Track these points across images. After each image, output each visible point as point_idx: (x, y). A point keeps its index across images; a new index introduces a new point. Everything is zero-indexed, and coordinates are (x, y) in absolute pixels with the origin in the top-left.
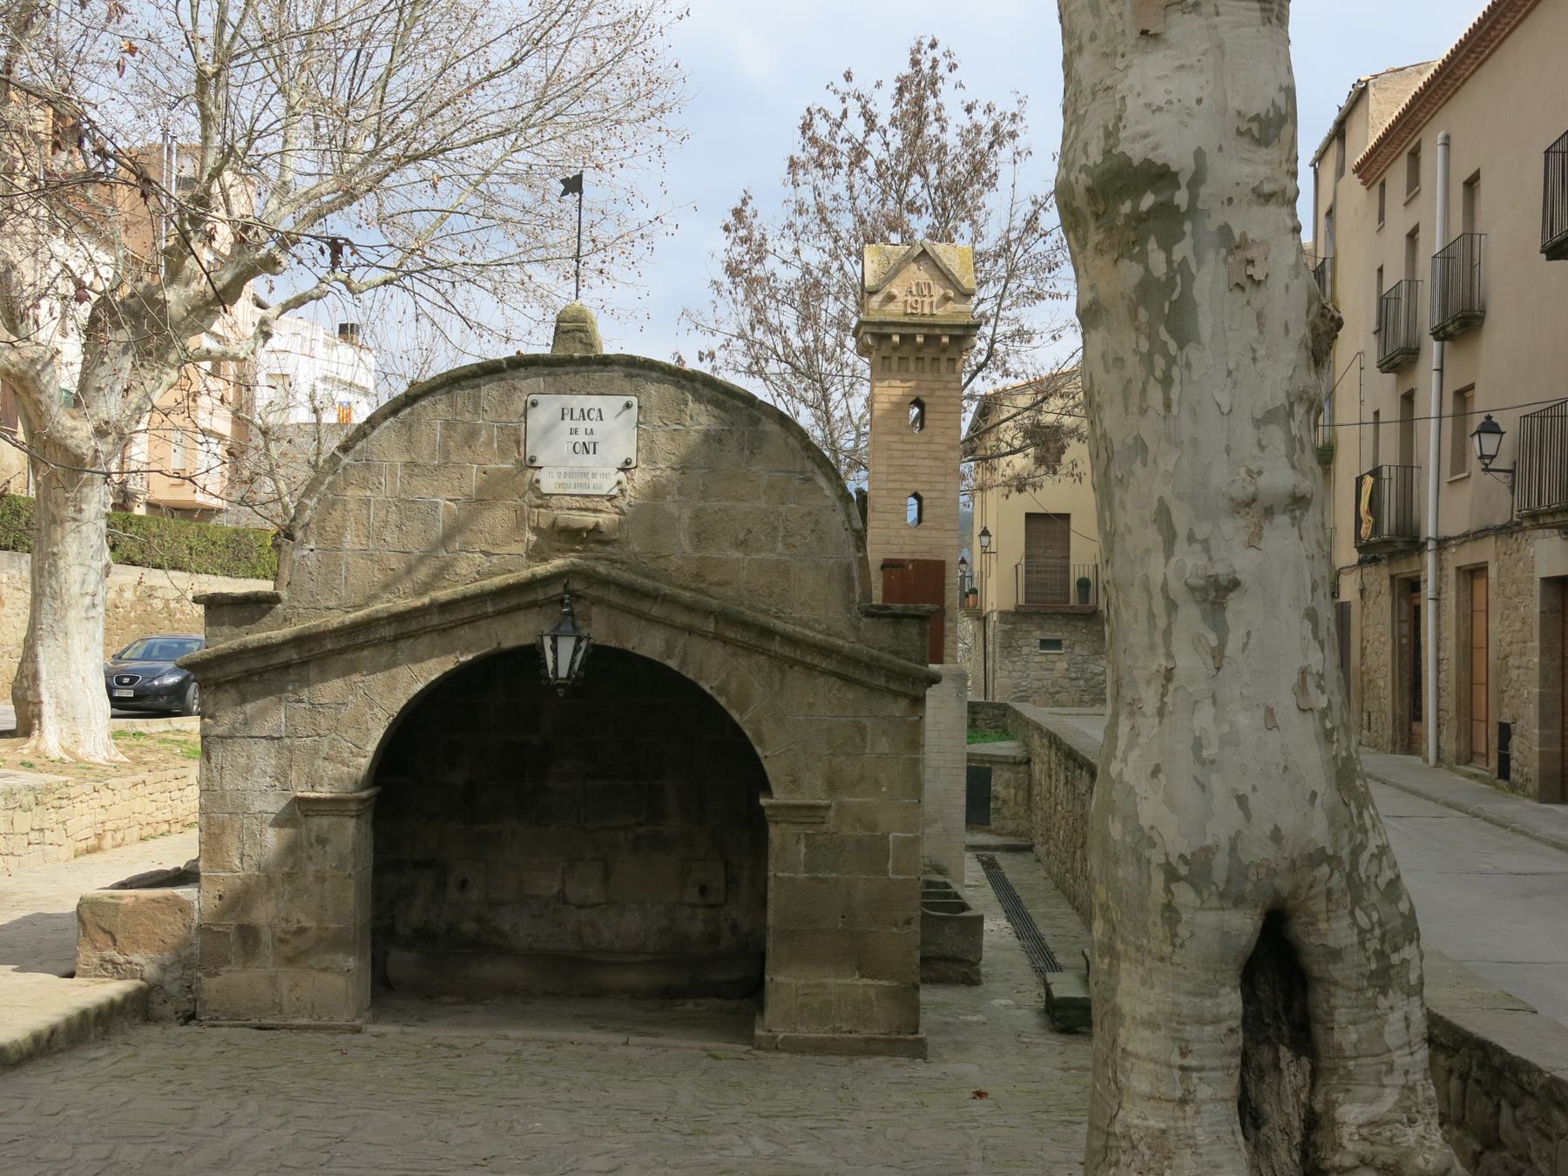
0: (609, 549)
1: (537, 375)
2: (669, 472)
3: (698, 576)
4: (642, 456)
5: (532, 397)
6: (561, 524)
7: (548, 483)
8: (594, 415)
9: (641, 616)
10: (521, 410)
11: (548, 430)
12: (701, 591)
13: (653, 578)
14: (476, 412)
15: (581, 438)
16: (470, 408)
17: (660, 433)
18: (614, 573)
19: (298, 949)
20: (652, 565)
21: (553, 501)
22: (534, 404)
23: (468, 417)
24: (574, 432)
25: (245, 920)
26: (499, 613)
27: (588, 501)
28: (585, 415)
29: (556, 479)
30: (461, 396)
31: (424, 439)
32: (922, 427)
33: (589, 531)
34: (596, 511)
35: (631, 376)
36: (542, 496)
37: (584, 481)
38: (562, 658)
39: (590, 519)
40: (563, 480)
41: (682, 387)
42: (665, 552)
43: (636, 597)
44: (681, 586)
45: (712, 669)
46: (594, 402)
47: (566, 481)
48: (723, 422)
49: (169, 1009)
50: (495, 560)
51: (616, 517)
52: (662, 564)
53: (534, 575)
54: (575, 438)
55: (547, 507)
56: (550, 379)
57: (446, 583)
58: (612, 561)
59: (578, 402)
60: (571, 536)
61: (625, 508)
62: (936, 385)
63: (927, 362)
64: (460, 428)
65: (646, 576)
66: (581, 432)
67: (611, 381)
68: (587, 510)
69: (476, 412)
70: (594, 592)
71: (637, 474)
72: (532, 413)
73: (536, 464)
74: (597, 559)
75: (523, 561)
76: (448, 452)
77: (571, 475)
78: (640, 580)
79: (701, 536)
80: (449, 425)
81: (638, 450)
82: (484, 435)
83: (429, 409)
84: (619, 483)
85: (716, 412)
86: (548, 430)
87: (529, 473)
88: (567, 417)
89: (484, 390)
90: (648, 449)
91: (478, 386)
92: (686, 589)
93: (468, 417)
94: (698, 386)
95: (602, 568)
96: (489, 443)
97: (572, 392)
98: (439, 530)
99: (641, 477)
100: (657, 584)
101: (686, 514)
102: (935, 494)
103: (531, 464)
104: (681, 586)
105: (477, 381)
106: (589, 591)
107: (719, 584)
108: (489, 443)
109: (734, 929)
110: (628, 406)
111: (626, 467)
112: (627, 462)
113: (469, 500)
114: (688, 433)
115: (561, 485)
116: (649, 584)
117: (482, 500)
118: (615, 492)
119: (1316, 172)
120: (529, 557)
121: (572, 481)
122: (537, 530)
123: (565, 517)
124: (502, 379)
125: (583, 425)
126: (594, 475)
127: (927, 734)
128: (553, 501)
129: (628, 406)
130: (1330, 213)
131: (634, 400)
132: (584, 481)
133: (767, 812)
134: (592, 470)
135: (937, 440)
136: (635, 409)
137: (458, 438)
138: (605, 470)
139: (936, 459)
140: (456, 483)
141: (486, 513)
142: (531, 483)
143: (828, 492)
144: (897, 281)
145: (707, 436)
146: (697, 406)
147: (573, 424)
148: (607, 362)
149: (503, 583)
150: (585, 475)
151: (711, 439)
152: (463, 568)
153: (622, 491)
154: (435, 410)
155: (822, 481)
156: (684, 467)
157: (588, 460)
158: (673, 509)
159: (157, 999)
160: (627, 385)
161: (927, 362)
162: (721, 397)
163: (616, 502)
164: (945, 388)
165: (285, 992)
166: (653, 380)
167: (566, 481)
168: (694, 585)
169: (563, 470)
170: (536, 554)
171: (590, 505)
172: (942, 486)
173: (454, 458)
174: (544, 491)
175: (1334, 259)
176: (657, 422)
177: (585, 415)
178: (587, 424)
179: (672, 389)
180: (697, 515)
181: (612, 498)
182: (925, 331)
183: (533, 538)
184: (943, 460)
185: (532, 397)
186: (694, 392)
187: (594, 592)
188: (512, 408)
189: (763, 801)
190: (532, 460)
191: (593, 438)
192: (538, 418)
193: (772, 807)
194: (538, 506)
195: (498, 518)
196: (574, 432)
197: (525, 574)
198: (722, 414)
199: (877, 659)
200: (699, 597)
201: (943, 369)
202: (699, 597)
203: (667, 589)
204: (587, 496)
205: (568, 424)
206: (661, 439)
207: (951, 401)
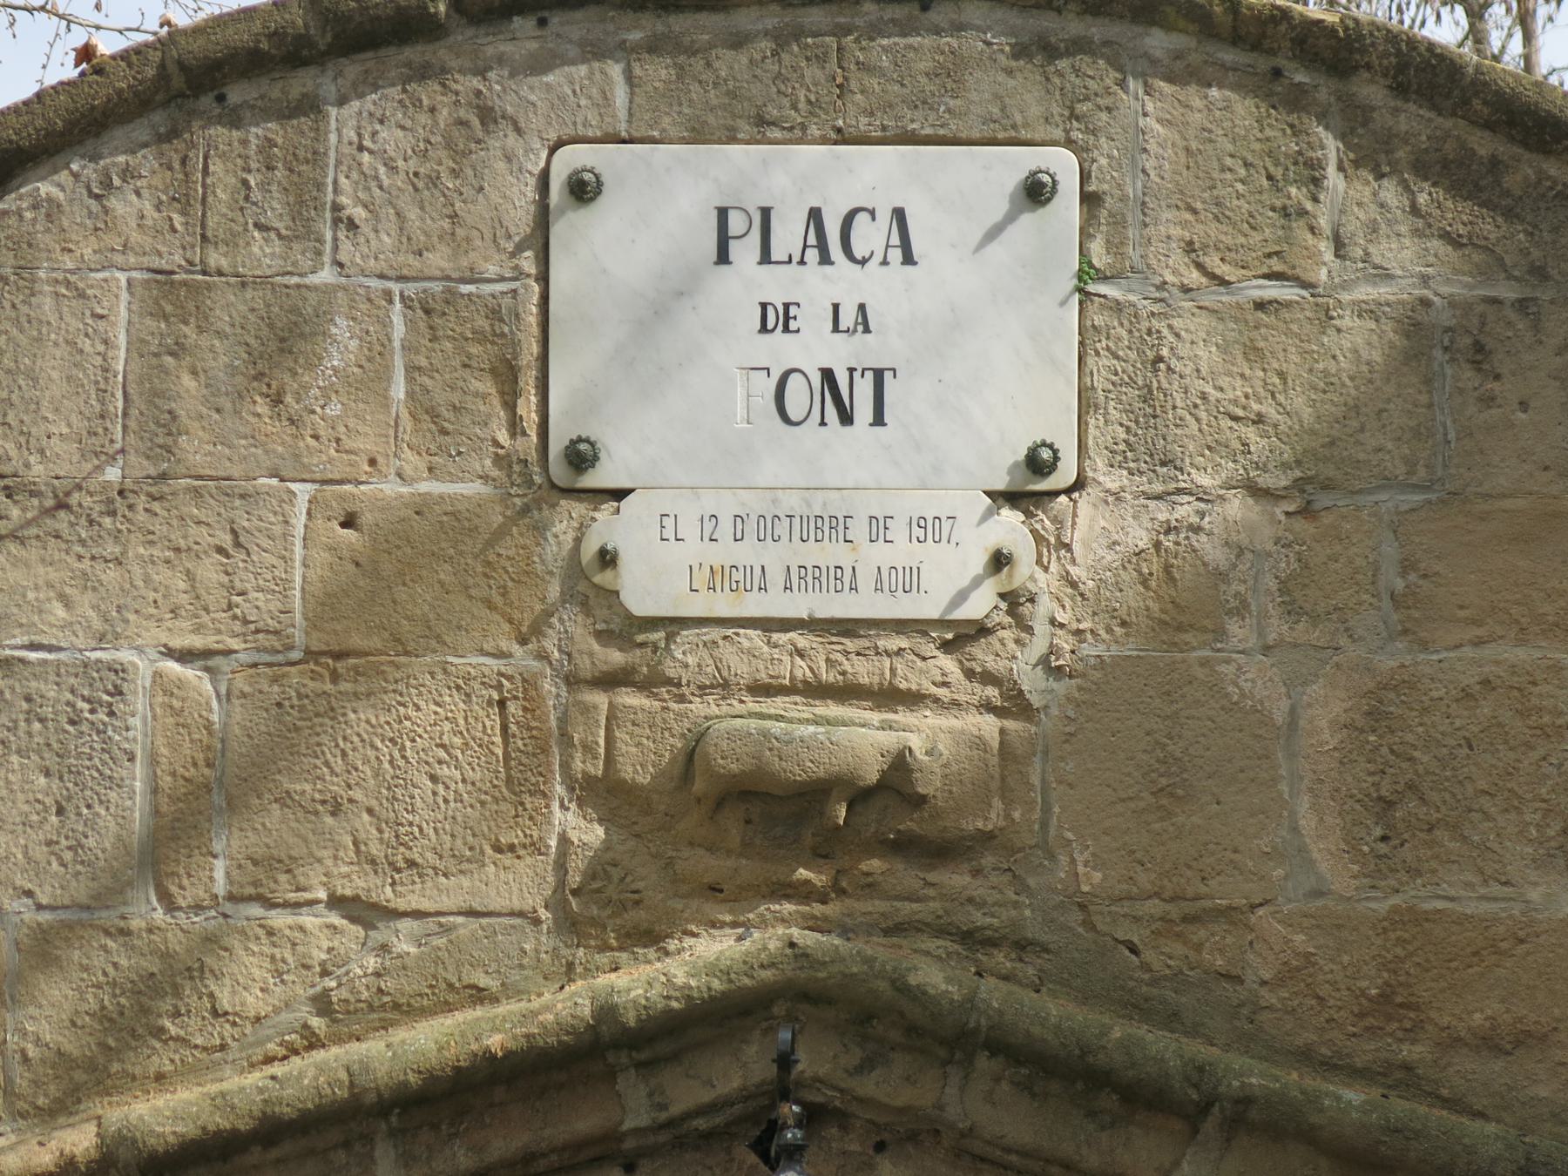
0: (956, 879)
1: (594, 51)
2: (1237, 506)
3: (1390, 1006)
4: (1107, 430)
5: (572, 158)
6: (727, 760)
7: (658, 568)
8: (871, 236)
10: (520, 218)
11: (663, 305)
12: (1402, 1078)
13: (1171, 1019)
14: (301, 230)
15: (812, 348)
16: (275, 210)
17: (1191, 323)
18: (992, 992)
20: (1163, 956)
21: (685, 656)
22: (583, 190)
23: (263, 253)
24: (777, 319)
27: (849, 653)
28: (826, 239)
29: (693, 550)
30: (227, 154)
31: (53, 365)
32: (908, 259)
33: (860, 796)
34: (889, 697)
35: (1046, 50)
36: (629, 629)
37: (829, 553)
39: (862, 740)
40: (726, 552)
41: (1296, 101)
42: (1226, 891)
44: (1305, 1057)
46: (870, 175)
47: (747, 553)
48: (1494, 264)
50: (403, 940)
51: (989, 726)
52: (1215, 948)
53: (606, 1012)
54: (782, 350)
55: (650, 683)
56: (657, 71)
57: (163, 1060)
58: (971, 939)
59: (798, 175)
60: (772, 820)
61: (1031, 681)
64: (228, 306)
65: (1138, 1008)
66: (812, 319)
67: (951, 73)
68: (847, 692)
69: (301, 230)
70: (895, 1087)
71: (1088, 522)
72: (569, 228)
73: (597, 478)
74: (897, 929)
75: (540, 942)
76: (171, 425)
77: (767, 528)
78: (1119, 1032)
79: (1395, 813)
80: (171, 295)
81: (1086, 403)
82: (342, 345)
83: (76, 216)
84: (999, 561)
85: (1459, 214)
86: (663, 305)
87: (564, 520)
88: (745, 251)
89: (342, 123)
90: (1131, 395)
91: (310, 106)
92: (1332, 1067)
93: (263, 253)
94: (1371, 91)
95: (935, 975)
96: (368, 380)
97: (763, 127)
98: (131, 804)
99: (1104, 530)
100: (1199, 1050)
101: (1326, 710)
103: (570, 475)
104: (1305, 1057)
105: (301, 83)
106: (868, 1086)
107: (1489, 1043)
108: (368, 380)
110: (1036, 192)
111: (1029, 488)
112: (1038, 463)
113: (275, 652)
114: (1326, 317)
115: (718, 577)
116: (1163, 1048)
117: (343, 652)
118: (981, 605)
120: (571, 926)
121: (774, 557)
122: (604, 794)
123: (737, 726)
124: (423, 73)
125: (817, 288)
126: (879, 527)
127: (425, 1024)
128: (685, 656)
129: (1036, 192)
131: (1062, 164)
132: (829, 553)
134: (866, 506)
136: (1067, 207)
137: (220, 356)
140: (209, 571)
141: (360, 718)
142: (574, 569)
145: (1418, 334)
146: (1364, 187)
147: (775, 285)
149: (458, 1054)
150: (833, 526)
151: (1443, 348)
152: (249, 984)
153: (1013, 600)
154: (104, 223)
156: (1309, 487)
157: (849, 454)
158: (1257, 682)
160: (1028, 93)
162: (1484, 145)
163: (983, 655)
166: (1151, 69)
168: (1366, 1052)
169: (727, 507)
170: (604, 910)
171: (864, 671)
173: (195, 450)
174: (639, 602)
176: (1177, 269)
177: (826, 239)
178: (840, 283)
179: (1244, 109)
180: (1377, 712)
181: (963, 636)
183: (590, 833)
185: (572, 158)
186: (1353, 122)
187: (895, 1087)
188: (475, 212)
190: (581, 457)
192: (604, 255)
194: (610, 681)
195: (429, 732)
196: (777, 319)
197: (562, 1005)
198: (1489, 227)
200: (1401, 1107)
202: (1401, 1107)
203: (1250, 1074)
204: (847, 628)
205: (748, 283)
206: (1197, 348)
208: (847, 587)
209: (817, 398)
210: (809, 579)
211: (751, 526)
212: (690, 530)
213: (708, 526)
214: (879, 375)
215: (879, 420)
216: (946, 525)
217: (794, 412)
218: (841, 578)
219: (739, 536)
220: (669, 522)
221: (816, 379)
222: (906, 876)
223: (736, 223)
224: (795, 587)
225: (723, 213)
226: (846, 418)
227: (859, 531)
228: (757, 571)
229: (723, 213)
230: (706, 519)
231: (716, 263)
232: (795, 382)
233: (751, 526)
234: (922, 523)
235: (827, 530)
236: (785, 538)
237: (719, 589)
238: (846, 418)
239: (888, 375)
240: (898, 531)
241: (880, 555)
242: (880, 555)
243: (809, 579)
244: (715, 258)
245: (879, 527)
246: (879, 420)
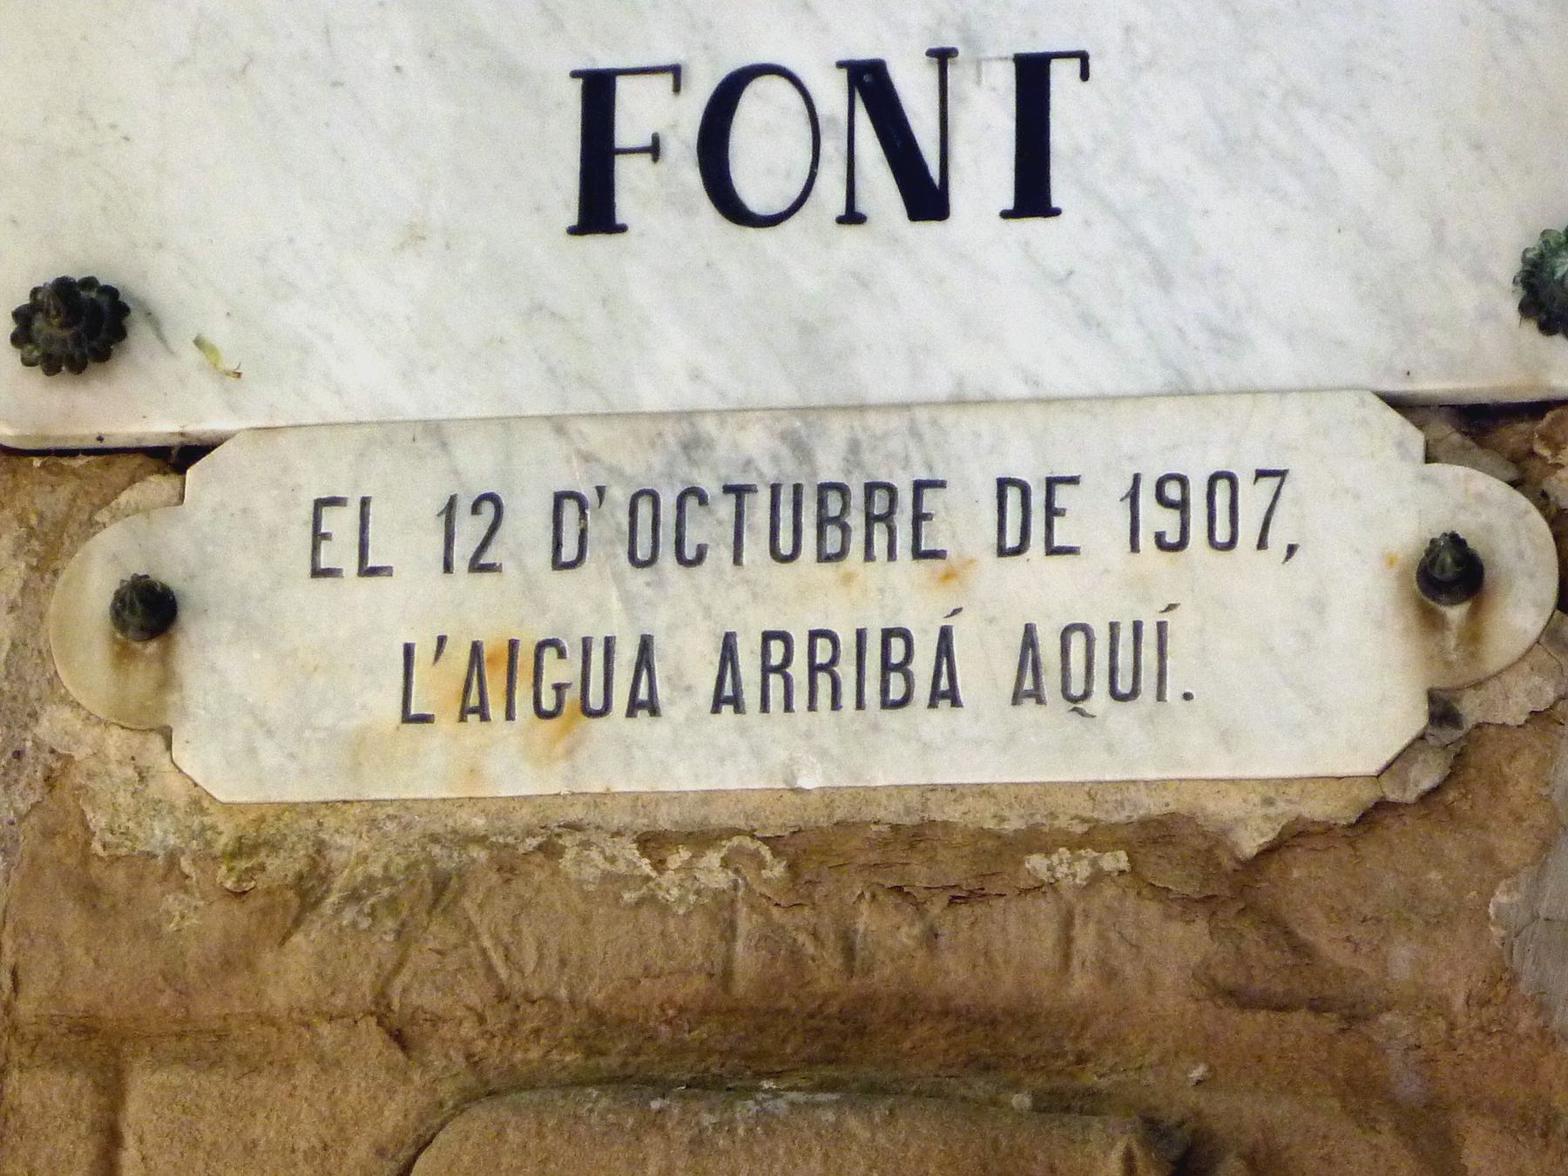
29: (420, 601)
40: (526, 600)
47: (597, 603)
77: (660, 530)
115: (489, 680)
121: (689, 617)
167: (597, 603)
208: (922, 690)
209: (833, 148)
210: (799, 669)
211: (608, 525)
212: (407, 539)
213: (469, 531)
214: (1032, 75)
215: (1032, 195)
216: (1253, 499)
217: (755, 192)
219: (569, 552)
220: (340, 523)
221: (832, 94)
223: (639, 111)
224: (751, 695)
225: (598, 91)
226: (926, 198)
227: (965, 521)
228: (626, 654)
229: (598, 91)
230: (464, 506)
231: (573, 231)
232: (762, 108)
233: (608, 525)
234: (1173, 491)
235: (856, 520)
236: (720, 554)
237: (496, 709)
238: (926, 198)
239: (1062, 75)
240: (1092, 519)
241: (1042, 592)
242: (1042, 592)
243: (799, 669)
244: (572, 217)
245: (1030, 513)
246: (1032, 195)
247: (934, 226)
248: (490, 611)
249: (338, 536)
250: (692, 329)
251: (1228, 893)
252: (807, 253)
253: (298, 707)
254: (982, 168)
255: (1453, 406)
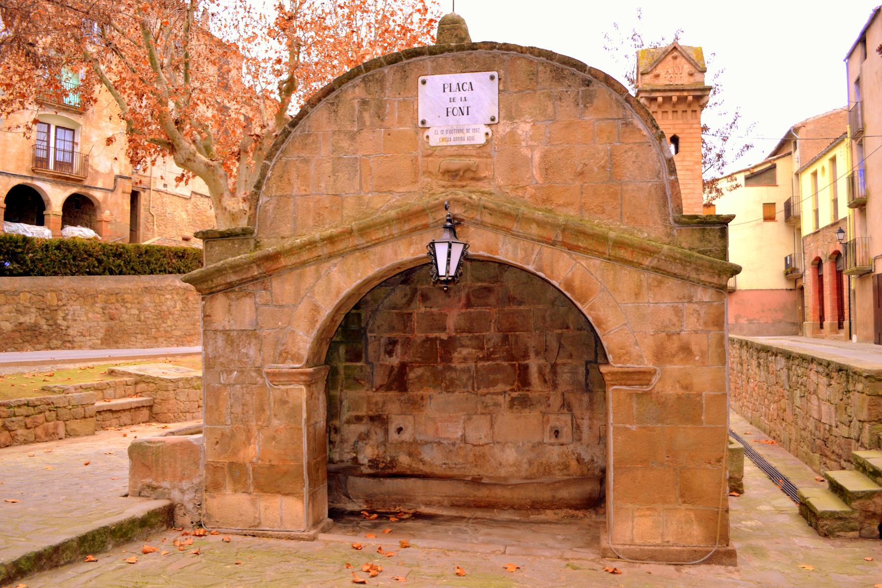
0: (480, 184)
8: (466, 87)
9: (508, 231)
15: (458, 104)
19: (269, 481)
25: (234, 460)
26: (402, 235)
28: (460, 87)
29: (440, 136)
38: (446, 261)
43: (506, 219)
45: (563, 269)
47: (448, 136)
49: (187, 520)
62: (686, 126)
63: (680, 113)
77: (451, 132)
88: (447, 90)
101: (537, 156)
102: (688, 191)
109: (579, 460)
115: (443, 139)
119: (847, 64)
121: (452, 136)
126: (468, 130)
130: (858, 82)
131: (495, 74)
133: (607, 378)
135: (688, 159)
138: (475, 127)
139: (687, 170)
143: (645, 133)
144: (660, 67)
147: (452, 95)
148: (474, 47)
150: (460, 131)
155: (638, 123)
157: (464, 120)
158: (526, 152)
159: (178, 512)
161: (680, 113)
164: (691, 128)
165: (262, 510)
167: (448, 136)
172: (692, 186)
175: (862, 102)
177: (460, 87)
178: (462, 94)
182: (678, 94)
184: (692, 170)
189: (603, 369)
191: (467, 104)
193: (613, 374)
196: (453, 100)
199: (690, 256)
201: (689, 117)
207: (695, 135)
218: (462, 139)
222: (473, 183)
223: (450, 110)
227: (465, 131)
241: (468, 135)
242: (468, 135)
245: (468, 130)
247: (3, 217)
248: (443, 136)
249: (436, 133)
250: (452, 121)
251: (152, 520)
252: (457, 117)
253: (435, 139)
254: (465, 113)
255: (78, 436)
